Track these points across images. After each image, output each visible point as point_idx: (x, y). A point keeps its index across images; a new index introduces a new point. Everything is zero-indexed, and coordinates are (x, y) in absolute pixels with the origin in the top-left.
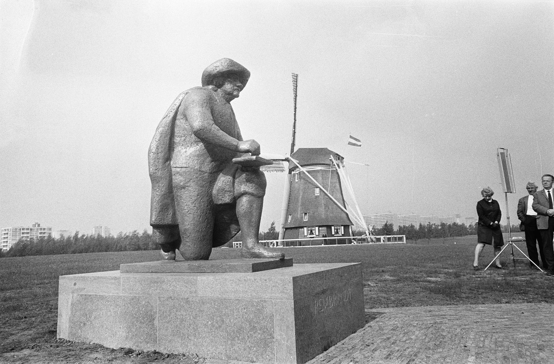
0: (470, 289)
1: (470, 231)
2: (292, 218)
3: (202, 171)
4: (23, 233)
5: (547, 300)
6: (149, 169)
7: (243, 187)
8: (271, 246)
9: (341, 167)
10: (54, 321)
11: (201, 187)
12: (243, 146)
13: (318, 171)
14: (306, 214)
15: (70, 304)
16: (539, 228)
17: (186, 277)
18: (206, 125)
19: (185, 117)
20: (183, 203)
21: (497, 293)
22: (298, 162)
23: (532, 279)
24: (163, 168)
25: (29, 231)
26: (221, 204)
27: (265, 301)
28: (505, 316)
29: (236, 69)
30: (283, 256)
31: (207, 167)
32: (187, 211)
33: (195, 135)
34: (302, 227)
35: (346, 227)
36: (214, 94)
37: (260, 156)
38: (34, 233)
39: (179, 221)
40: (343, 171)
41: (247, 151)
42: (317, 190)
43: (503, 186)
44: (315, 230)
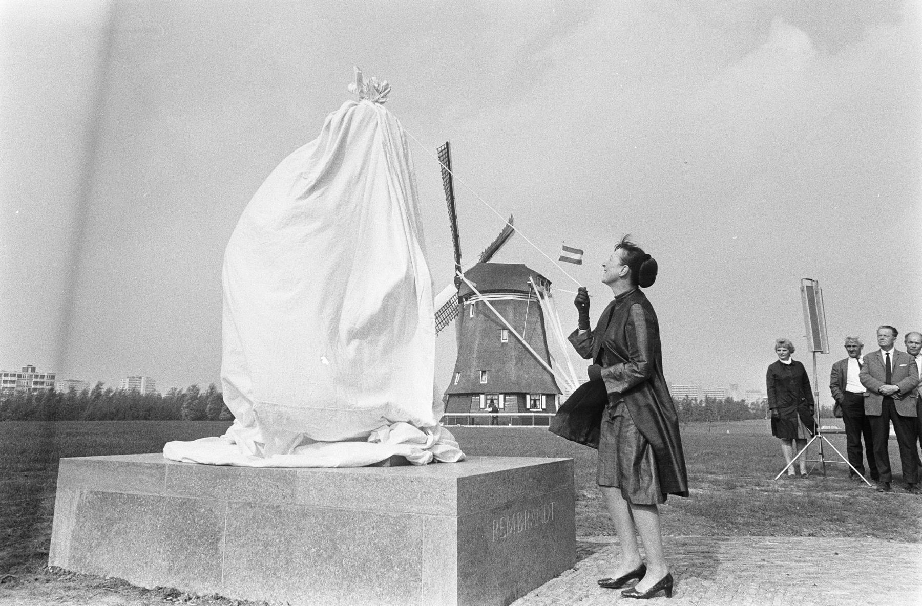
4: (5, 382)
5: (876, 532)
9: (546, 297)
13: (507, 302)
14: (484, 372)
15: (75, 504)
16: (867, 413)
21: (795, 518)
23: (854, 497)
25: (16, 379)
34: (478, 394)
40: (548, 304)
42: (505, 334)
43: (809, 340)
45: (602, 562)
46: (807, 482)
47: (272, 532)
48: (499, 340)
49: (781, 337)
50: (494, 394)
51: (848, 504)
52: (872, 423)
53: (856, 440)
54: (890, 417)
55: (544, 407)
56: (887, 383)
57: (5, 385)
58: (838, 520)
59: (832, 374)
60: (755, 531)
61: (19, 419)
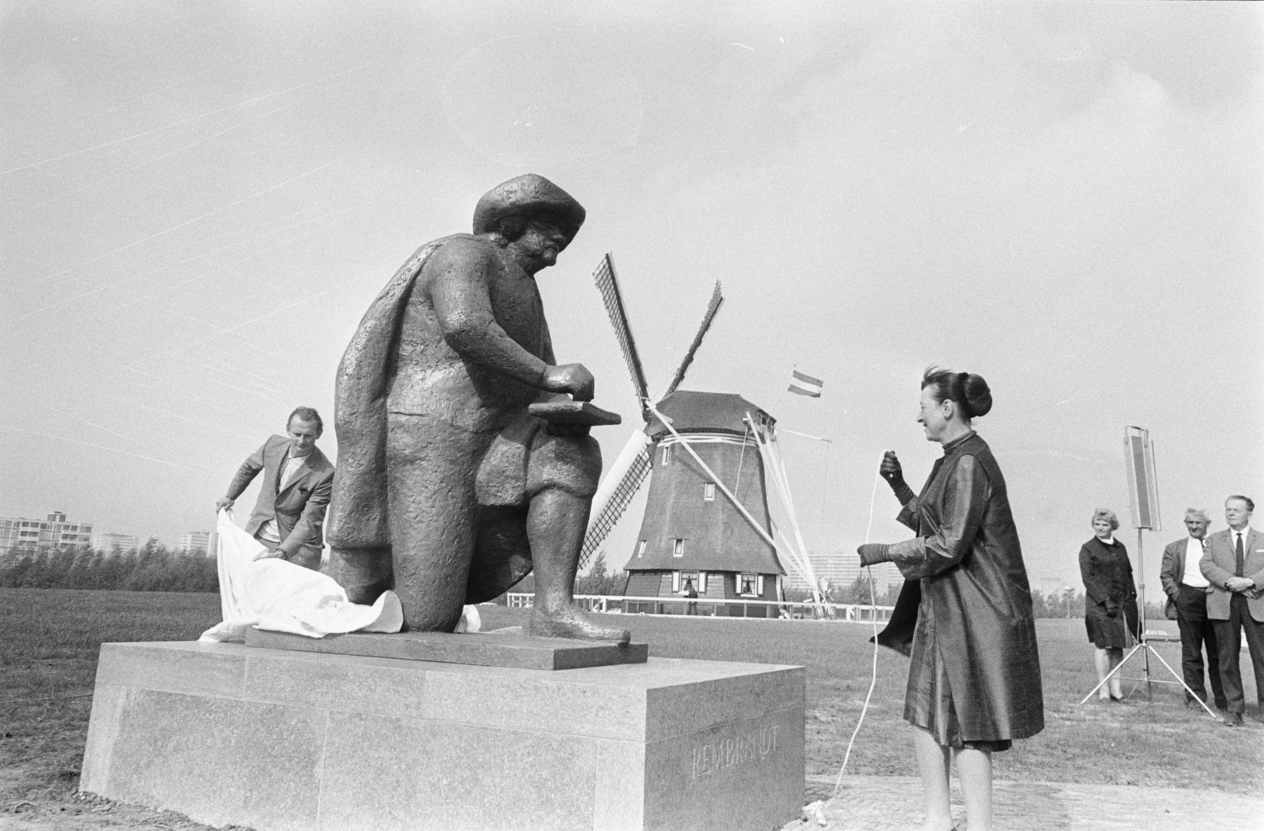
0: (1048, 746)
1: (1049, 608)
2: (647, 548)
3: (458, 428)
4: (23, 534)
5: (1222, 783)
6: (336, 411)
7: (549, 468)
8: (594, 610)
9: (768, 441)
10: (77, 748)
11: (452, 462)
12: (558, 378)
13: (715, 445)
14: (679, 541)
15: (119, 710)
16: (1209, 617)
17: (399, 669)
18: (476, 322)
19: (430, 299)
20: (406, 496)
21: (1110, 759)
22: (671, 420)
23: (1193, 731)
24: (370, 411)
25: (38, 530)
26: (493, 506)
27: (579, 741)
28: (1127, 817)
29: (552, 201)
30: (627, 637)
31: (471, 416)
32: (412, 515)
33: (448, 342)
34: (670, 571)
35: (770, 578)
36: (499, 252)
37: (592, 402)
38: (50, 535)
39: (394, 536)
40: (771, 450)
41: (564, 390)
42: (710, 489)
43: (1133, 512)
44: (697, 580)
45: (841, 811)
46: (1125, 708)
47: (388, 754)
48: (702, 498)
49: (1102, 508)
50: (693, 572)
51: (1182, 743)
52: (1217, 628)
53: (1195, 654)
54: (1241, 622)
55: (761, 592)
56: (1237, 575)
57: (24, 538)
58: (1170, 764)
59: (1165, 558)
60: (1052, 775)
61: (39, 585)
